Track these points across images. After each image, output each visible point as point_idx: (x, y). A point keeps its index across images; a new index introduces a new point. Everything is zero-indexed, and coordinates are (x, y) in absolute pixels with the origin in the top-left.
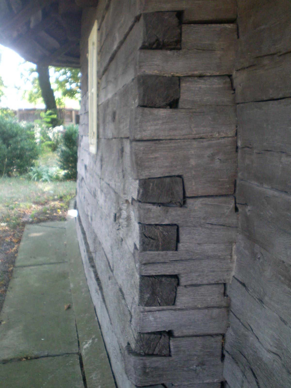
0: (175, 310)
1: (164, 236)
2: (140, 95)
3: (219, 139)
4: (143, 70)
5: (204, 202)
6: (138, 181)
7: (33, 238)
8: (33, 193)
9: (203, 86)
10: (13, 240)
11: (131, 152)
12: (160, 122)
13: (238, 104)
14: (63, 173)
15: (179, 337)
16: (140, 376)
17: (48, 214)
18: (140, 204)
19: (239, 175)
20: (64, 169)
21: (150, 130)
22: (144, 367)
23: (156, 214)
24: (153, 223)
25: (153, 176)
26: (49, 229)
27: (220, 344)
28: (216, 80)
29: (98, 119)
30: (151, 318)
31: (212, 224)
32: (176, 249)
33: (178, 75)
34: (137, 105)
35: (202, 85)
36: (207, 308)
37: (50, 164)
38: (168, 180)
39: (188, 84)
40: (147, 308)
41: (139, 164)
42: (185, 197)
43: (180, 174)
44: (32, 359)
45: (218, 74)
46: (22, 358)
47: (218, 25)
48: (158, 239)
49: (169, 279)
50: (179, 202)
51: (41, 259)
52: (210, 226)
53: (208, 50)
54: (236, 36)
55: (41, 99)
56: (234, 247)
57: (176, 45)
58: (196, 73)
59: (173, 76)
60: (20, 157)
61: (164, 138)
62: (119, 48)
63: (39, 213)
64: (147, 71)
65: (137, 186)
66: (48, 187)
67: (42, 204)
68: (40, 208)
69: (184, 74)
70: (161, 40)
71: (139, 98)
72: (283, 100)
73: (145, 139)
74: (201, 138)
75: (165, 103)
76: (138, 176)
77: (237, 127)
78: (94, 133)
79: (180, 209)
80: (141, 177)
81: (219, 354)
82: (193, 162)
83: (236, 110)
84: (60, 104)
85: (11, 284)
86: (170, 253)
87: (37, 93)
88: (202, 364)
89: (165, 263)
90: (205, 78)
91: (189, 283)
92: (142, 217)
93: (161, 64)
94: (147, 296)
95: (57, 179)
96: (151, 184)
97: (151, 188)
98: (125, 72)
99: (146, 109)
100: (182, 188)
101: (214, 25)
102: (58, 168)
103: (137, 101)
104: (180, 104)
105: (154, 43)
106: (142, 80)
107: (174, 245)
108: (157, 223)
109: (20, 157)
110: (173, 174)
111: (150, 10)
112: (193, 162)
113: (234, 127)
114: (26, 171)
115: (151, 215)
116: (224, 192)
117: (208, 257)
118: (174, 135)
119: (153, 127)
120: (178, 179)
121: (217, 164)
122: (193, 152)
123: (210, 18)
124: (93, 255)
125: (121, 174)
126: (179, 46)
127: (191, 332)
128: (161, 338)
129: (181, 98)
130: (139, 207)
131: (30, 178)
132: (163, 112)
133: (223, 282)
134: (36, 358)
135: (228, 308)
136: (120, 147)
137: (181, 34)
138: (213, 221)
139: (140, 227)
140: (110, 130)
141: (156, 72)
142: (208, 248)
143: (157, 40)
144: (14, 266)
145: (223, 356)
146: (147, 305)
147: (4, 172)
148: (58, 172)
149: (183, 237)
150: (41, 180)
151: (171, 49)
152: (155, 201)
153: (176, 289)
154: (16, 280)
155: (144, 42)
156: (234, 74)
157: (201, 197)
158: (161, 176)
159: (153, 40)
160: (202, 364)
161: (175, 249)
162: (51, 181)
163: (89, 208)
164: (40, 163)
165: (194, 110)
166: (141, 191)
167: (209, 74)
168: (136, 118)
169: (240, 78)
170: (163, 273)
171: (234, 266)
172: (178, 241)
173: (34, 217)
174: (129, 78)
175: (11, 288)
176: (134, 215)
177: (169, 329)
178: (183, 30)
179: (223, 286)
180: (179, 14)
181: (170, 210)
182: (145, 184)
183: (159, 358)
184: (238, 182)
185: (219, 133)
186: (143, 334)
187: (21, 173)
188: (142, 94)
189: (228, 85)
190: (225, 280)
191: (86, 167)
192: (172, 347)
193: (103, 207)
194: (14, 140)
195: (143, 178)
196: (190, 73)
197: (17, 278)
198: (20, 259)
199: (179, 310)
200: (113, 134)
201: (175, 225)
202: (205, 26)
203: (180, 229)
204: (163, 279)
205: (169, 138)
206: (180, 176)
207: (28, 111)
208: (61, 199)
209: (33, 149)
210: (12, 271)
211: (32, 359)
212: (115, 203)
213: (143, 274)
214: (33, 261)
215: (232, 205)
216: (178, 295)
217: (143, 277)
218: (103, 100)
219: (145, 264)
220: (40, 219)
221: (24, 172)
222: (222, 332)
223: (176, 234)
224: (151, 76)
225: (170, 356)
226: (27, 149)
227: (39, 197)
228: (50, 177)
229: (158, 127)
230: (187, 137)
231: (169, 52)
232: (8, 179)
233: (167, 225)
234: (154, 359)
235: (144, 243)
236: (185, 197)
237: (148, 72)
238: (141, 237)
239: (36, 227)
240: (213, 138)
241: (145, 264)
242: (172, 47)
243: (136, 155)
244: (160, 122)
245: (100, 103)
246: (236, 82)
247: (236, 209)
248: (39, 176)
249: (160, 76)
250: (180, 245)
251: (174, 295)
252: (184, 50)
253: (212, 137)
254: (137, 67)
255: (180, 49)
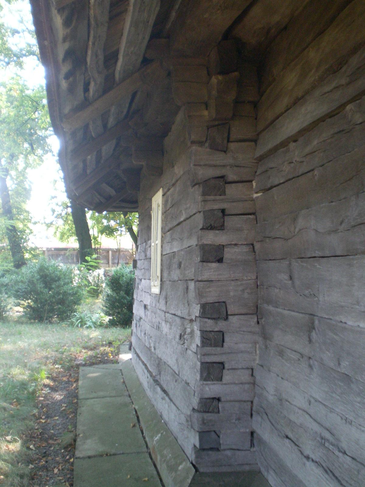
0: (222, 384)
1: (215, 338)
2: (201, 255)
3: (246, 280)
4: (202, 241)
5: (238, 318)
6: (199, 305)
7: (89, 378)
8: (79, 339)
9: (237, 250)
10: (71, 380)
11: (195, 288)
12: (213, 270)
13: (257, 260)
14: (107, 319)
15: (224, 401)
16: (201, 425)
17: (99, 357)
18: (201, 319)
19: (259, 302)
20: (109, 315)
21: (206, 275)
22: (203, 420)
23: (210, 324)
24: (208, 330)
25: (208, 302)
26: (104, 370)
27: (250, 407)
28: (244, 247)
29: (162, 265)
30: (207, 389)
31: (244, 331)
32: (222, 346)
33: (222, 244)
34: (199, 261)
35: (236, 249)
36: (242, 383)
37: (95, 310)
38: (217, 304)
39: (228, 249)
40: (205, 382)
41: (200, 294)
42: (227, 315)
43: (224, 301)
44: (110, 455)
45: (246, 243)
46: (103, 455)
47: (245, 216)
48: (212, 340)
49: (218, 365)
50: (224, 318)
51: (101, 394)
52: (242, 332)
53: (240, 230)
54: (255, 222)
55: (75, 238)
56: (257, 346)
57: (222, 227)
58: (233, 243)
59: (220, 245)
60: (62, 302)
61: (215, 279)
62: (185, 220)
63: (91, 357)
64: (205, 242)
65: (199, 308)
66: (95, 334)
67: (91, 350)
68: (90, 353)
69: (226, 243)
70: (213, 225)
71: (200, 257)
72: (274, 261)
73: (203, 280)
74: (237, 280)
75: (215, 260)
76: (200, 302)
77: (257, 273)
78: (158, 277)
79: (225, 322)
80: (201, 303)
81: (250, 414)
82: (232, 294)
83: (256, 264)
84: (97, 242)
85: (79, 411)
86: (219, 349)
87: (69, 230)
88: (239, 419)
89: (215, 355)
90: (238, 246)
91: (230, 367)
92: (202, 326)
93: (214, 238)
94: (205, 375)
95: (101, 325)
96: (207, 307)
97: (207, 309)
98: (190, 237)
99: (204, 263)
100: (225, 309)
101: (243, 216)
102: (102, 314)
103: (199, 258)
104: (224, 260)
105: (209, 227)
106: (202, 248)
107: (221, 344)
108: (211, 330)
109: (62, 302)
110: (220, 301)
111: (207, 209)
112: (232, 294)
113: (255, 274)
114: (68, 317)
115: (207, 325)
116: (251, 312)
117: (242, 352)
118: (221, 278)
119: (208, 274)
120: (223, 304)
121: (246, 295)
122: (231, 288)
123: (241, 213)
124: (158, 378)
125: (186, 304)
126: (223, 228)
127: (232, 399)
128: (213, 401)
129: (225, 256)
130: (200, 320)
131: (72, 324)
132: (214, 265)
133: (251, 367)
134: (114, 455)
135: (254, 384)
136: (186, 286)
137: (224, 221)
138: (245, 329)
139: (200, 333)
140: (176, 274)
141: (210, 242)
142: (242, 346)
143: (211, 225)
144: (78, 399)
145: (252, 415)
146: (205, 380)
147: (45, 318)
148: (102, 319)
149: (227, 339)
150: (85, 327)
151: (219, 230)
152: (209, 316)
153: (222, 371)
154: (83, 409)
155: (203, 226)
156: (255, 243)
157: (237, 315)
158: (213, 302)
159: (209, 225)
160: (239, 419)
161: (221, 346)
162: (95, 327)
163: (152, 340)
164: (82, 310)
165: (232, 264)
166: (201, 311)
167: (240, 243)
168: (198, 268)
169: (257, 246)
170: (214, 361)
171: (257, 357)
172: (223, 341)
173: (85, 360)
174: (193, 242)
175: (80, 414)
176: (196, 328)
177: (219, 396)
178: (225, 219)
179: (251, 370)
180: (223, 211)
181: (219, 322)
182: (204, 307)
183: (213, 414)
184: (259, 306)
185: (247, 277)
186: (202, 399)
187: (62, 319)
188: (202, 255)
189: (251, 249)
190: (252, 366)
191: (145, 307)
192: (220, 408)
193: (168, 334)
194: (57, 283)
195: (203, 303)
196: (229, 243)
197: (83, 407)
198: (82, 393)
199: (225, 384)
200: (179, 278)
201: (222, 331)
202: (238, 216)
203: (225, 334)
204: (215, 365)
205: (217, 279)
206: (224, 302)
207: (58, 250)
208: (110, 344)
209: (76, 294)
210: (77, 403)
211: (110, 455)
212: (181, 326)
213: (203, 361)
214: (94, 395)
215: (256, 320)
216: (223, 375)
217: (202, 363)
218: (168, 250)
219: (204, 355)
220: (92, 362)
221: (66, 319)
222: (251, 400)
223: (222, 338)
224: (207, 245)
225: (219, 412)
226: (70, 294)
227: (87, 342)
228: (94, 323)
229: (211, 273)
230: (228, 279)
231: (217, 232)
232: (50, 326)
233: (217, 331)
234: (209, 414)
235: (203, 342)
236: (227, 315)
237: (205, 242)
238: (201, 338)
239: (91, 369)
240: (243, 280)
241: (204, 355)
242: (220, 228)
243: (199, 289)
244: (213, 270)
245: (164, 253)
246: (256, 248)
247: (258, 323)
248: (83, 323)
249: (212, 245)
250: (225, 344)
251: (221, 374)
252: (226, 230)
253: (243, 280)
254: (200, 239)
255: (224, 229)
